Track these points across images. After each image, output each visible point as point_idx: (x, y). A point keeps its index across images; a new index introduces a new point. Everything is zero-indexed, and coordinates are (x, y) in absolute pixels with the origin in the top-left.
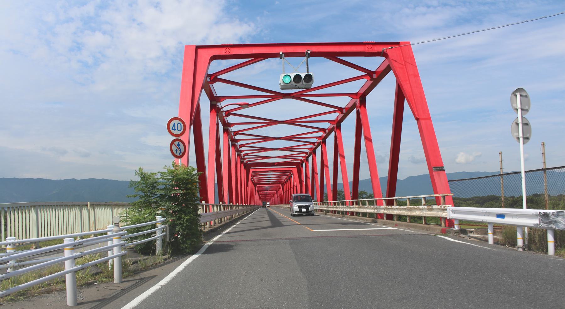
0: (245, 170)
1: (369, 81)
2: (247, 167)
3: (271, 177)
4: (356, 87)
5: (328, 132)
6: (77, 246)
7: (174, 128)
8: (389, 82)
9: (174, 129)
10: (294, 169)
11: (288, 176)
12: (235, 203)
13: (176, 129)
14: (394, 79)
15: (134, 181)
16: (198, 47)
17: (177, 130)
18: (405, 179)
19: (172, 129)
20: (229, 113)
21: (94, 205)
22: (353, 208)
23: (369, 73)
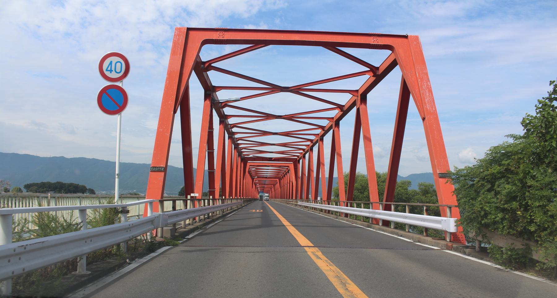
0: (235, 150)
1: (322, 131)
2: (245, 160)
3: (268, 171)
4: (358, 83)
5: (325, 130)
7: (109, 69)
8: (396, 75)
9: (109, 71)
10: (291, 165)
11: (285, 171)
12: (227, 197)
13: (112, 71)
14: (400, 74)
16: (189, 29)
17: (114, 72)
18: (407, 177)
19: (107, 70)
21: (81, 198)
22: (300, 203)
23: (373, 69)
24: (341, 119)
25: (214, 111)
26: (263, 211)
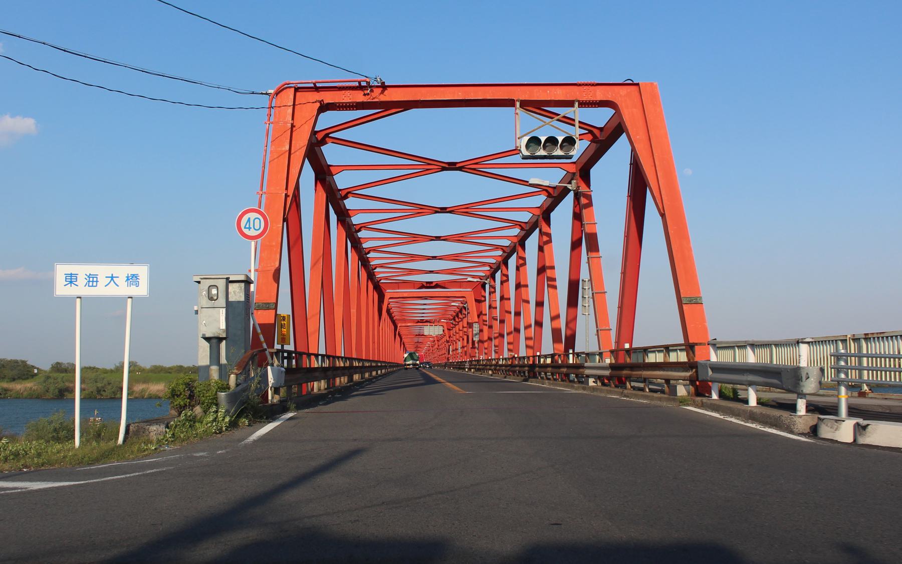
0: (353, 249)
6: (377, 91)
7: (248, 226)
8: (619, 153)
9: (247, 228)
13: (251, 228)
15: (148, 367)
17: (252, 229)
19: (245, 228)
20: (349, 193)
24: (553, 210)
25: (370, 282)
26: (324, 379)
